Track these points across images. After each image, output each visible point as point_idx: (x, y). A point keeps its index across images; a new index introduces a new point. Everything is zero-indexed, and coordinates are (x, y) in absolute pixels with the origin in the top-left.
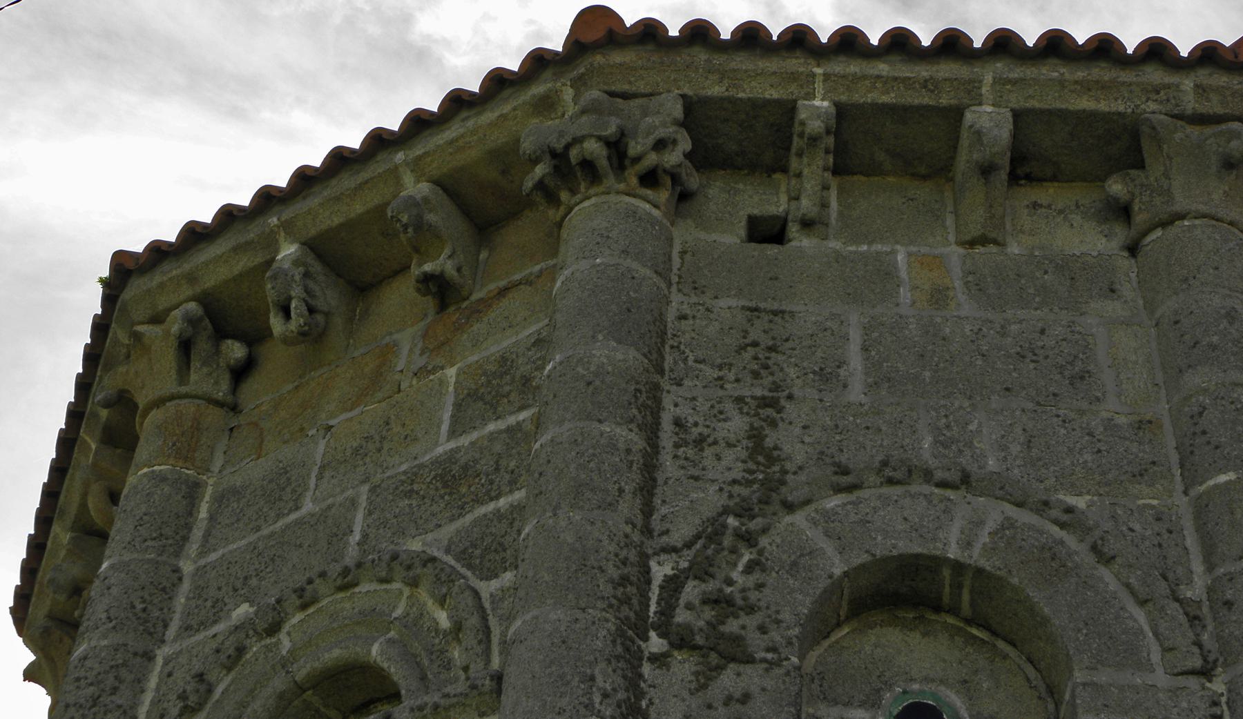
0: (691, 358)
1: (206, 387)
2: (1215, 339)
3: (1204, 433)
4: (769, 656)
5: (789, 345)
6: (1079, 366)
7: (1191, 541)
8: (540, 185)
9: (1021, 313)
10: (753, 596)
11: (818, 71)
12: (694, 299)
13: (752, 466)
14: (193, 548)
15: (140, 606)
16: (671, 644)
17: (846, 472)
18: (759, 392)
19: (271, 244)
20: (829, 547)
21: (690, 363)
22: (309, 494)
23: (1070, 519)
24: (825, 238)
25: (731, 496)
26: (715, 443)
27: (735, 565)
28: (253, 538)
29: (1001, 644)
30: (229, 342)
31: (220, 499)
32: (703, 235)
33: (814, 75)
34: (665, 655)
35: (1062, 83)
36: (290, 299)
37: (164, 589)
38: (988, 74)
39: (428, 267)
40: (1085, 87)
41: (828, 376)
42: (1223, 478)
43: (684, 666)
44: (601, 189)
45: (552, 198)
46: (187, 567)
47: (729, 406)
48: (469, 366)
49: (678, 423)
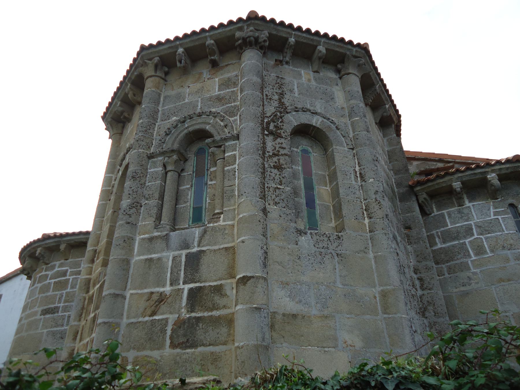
0: (267, 83)
1: (160, 75)
2: (356, 95)
3: (353, 111)
4: (285, 137)
5: (284, 84)
6: (332, 97)
7: (350, 128)
8: (240, 45)
9: (323, 86)
10: (282, 127)
11: (293, 33)
12: (267, 73)
13: (279, 105)
14: (161, 105)
15: (152, 115)
16: (269, 133)
17: (297, 108)
18: (280, 92)
19: (177, 47)
20: (294, 121)
21: (267, 84)
22: (187, 99)
23: (333, 122)
24: (289, 66)
25: (276, 109)
26: (273, 100)
27: (279, 121)
28: (175, 105)
29: (317, 141)
30: (164, 67)
31: (165, 97)
32: (268, 61)
33: (292, 33)
34: (268, 134)
35: (334, 45)
36: (182, 59)
37: (156, 112)
38: (323, 40)
39: (212, 58)
40: (338, 46)
41: (291, 91)
42: (357, 118)
43: (271, 138)
44: (252, 48)
45: (241, 49)
46: (160, 109)
47: (275, 93)
48: (221, 78)
49: (266, 95)
